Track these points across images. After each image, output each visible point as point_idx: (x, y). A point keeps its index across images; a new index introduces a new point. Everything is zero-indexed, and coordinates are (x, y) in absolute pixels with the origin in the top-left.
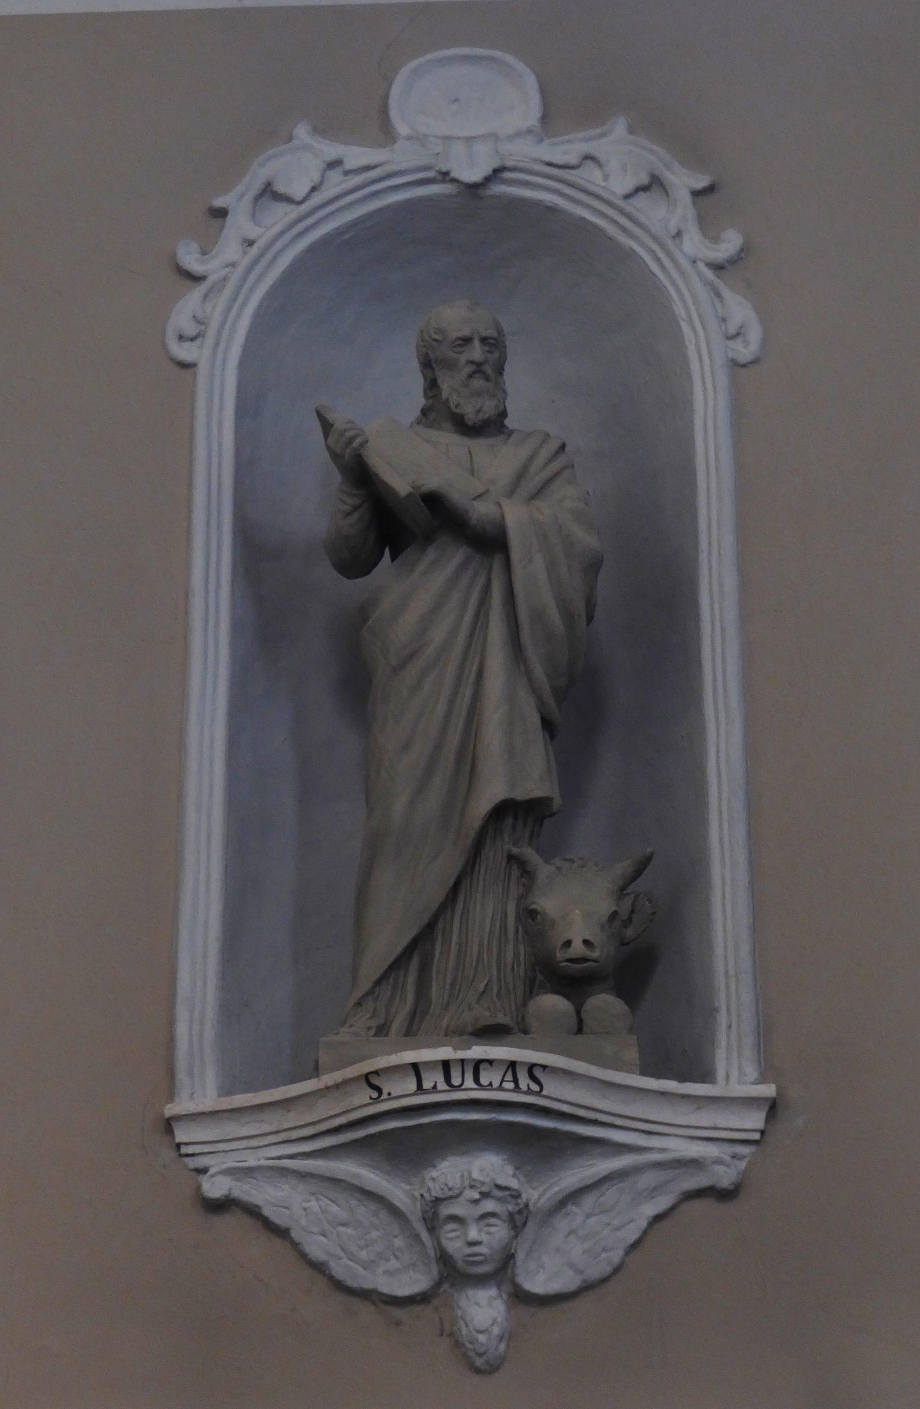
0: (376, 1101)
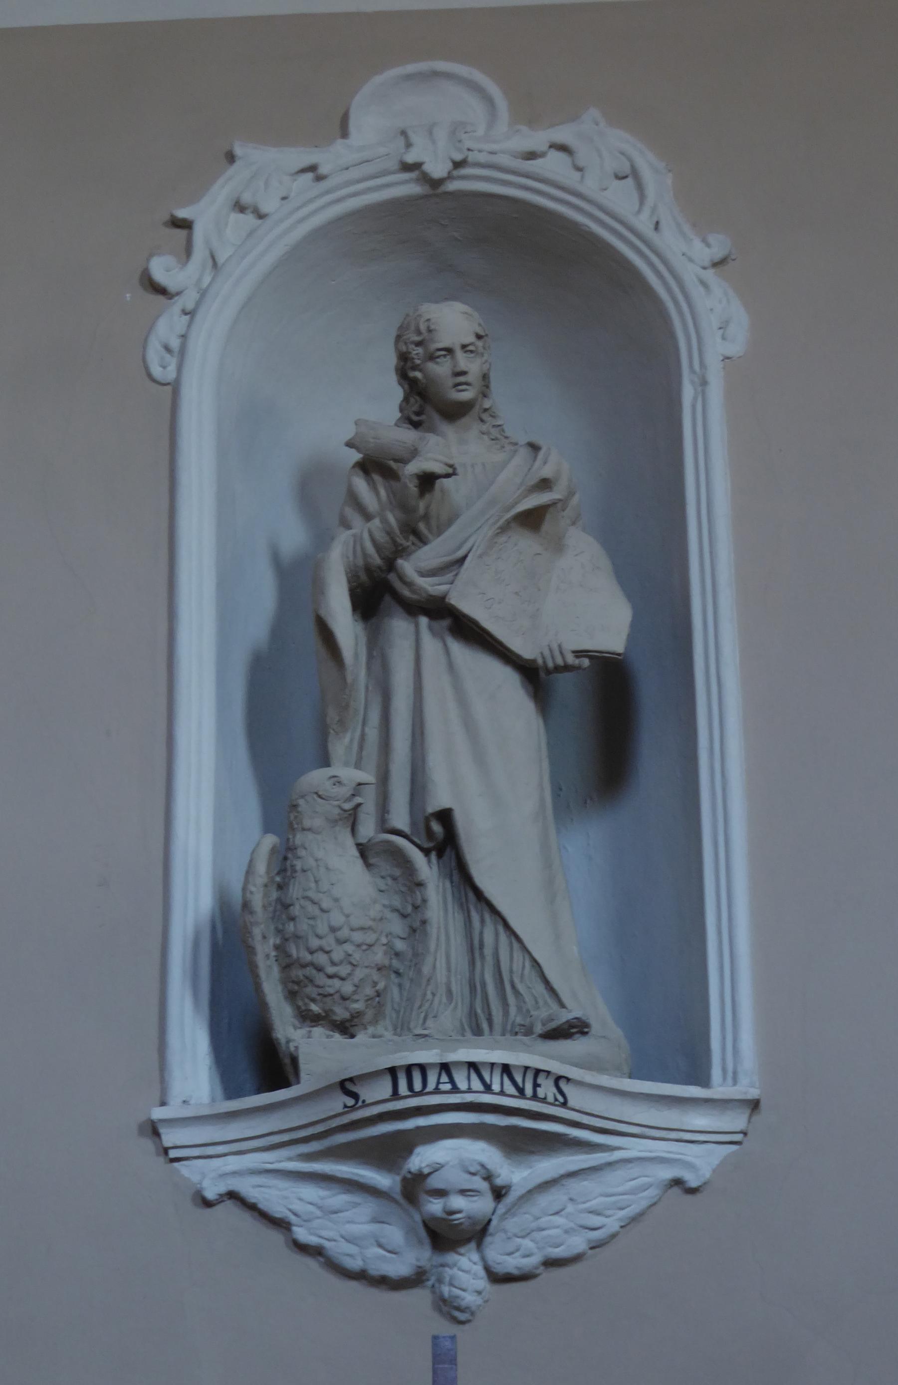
0: (353, 1108)
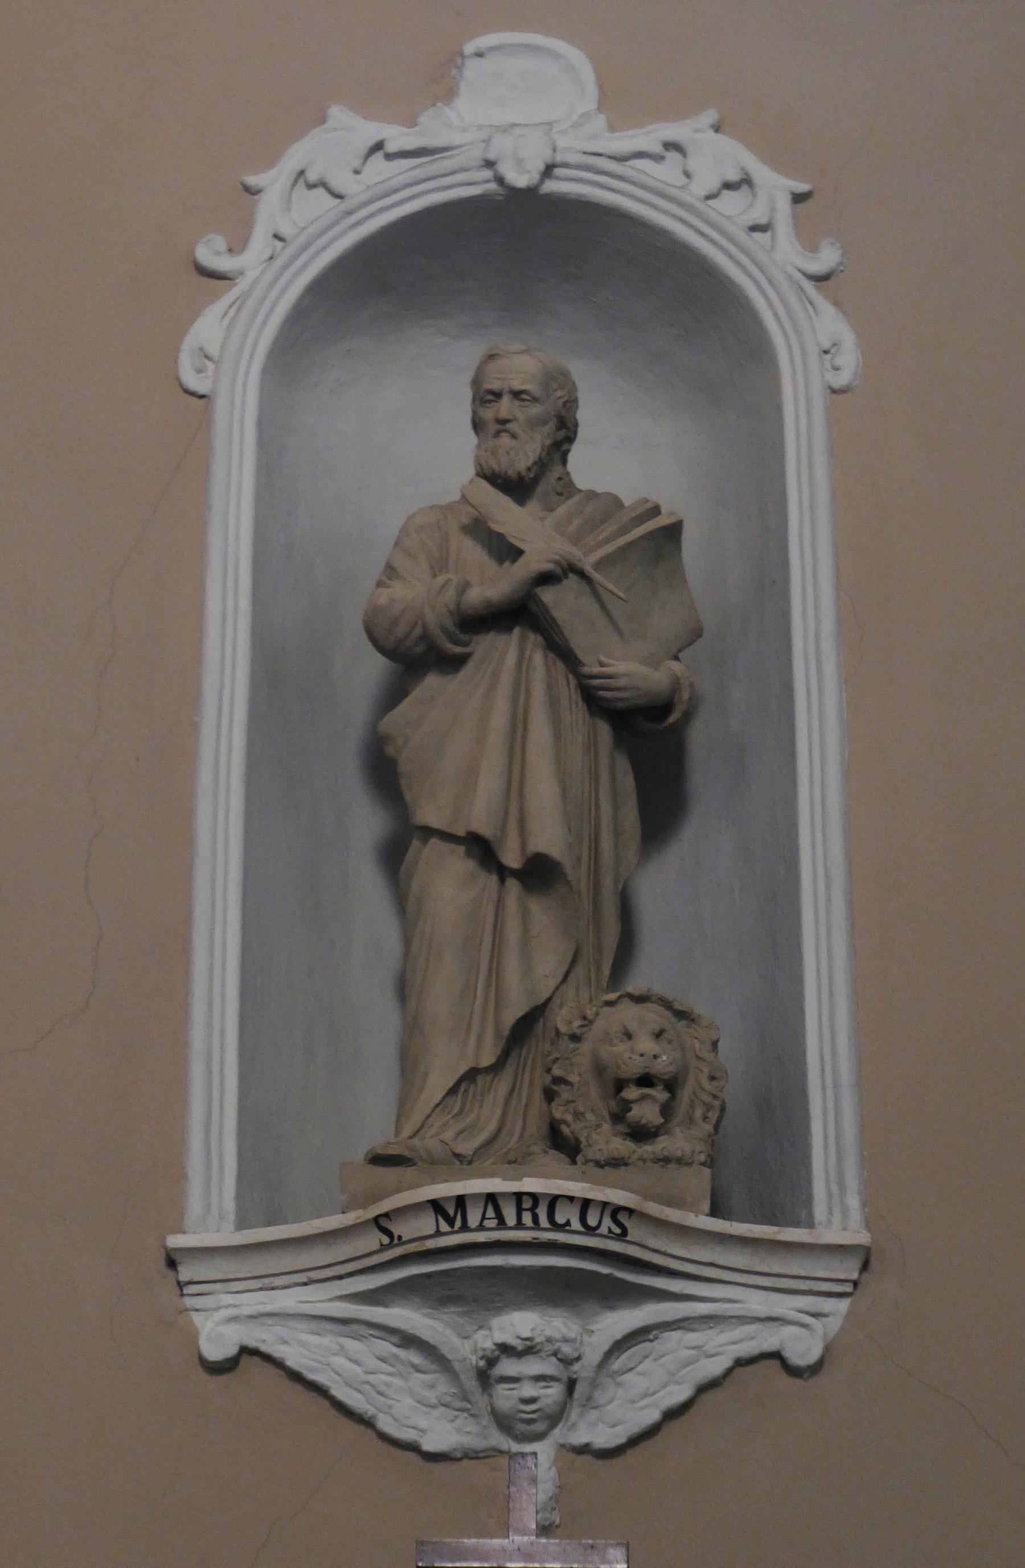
0: (390, 1246)
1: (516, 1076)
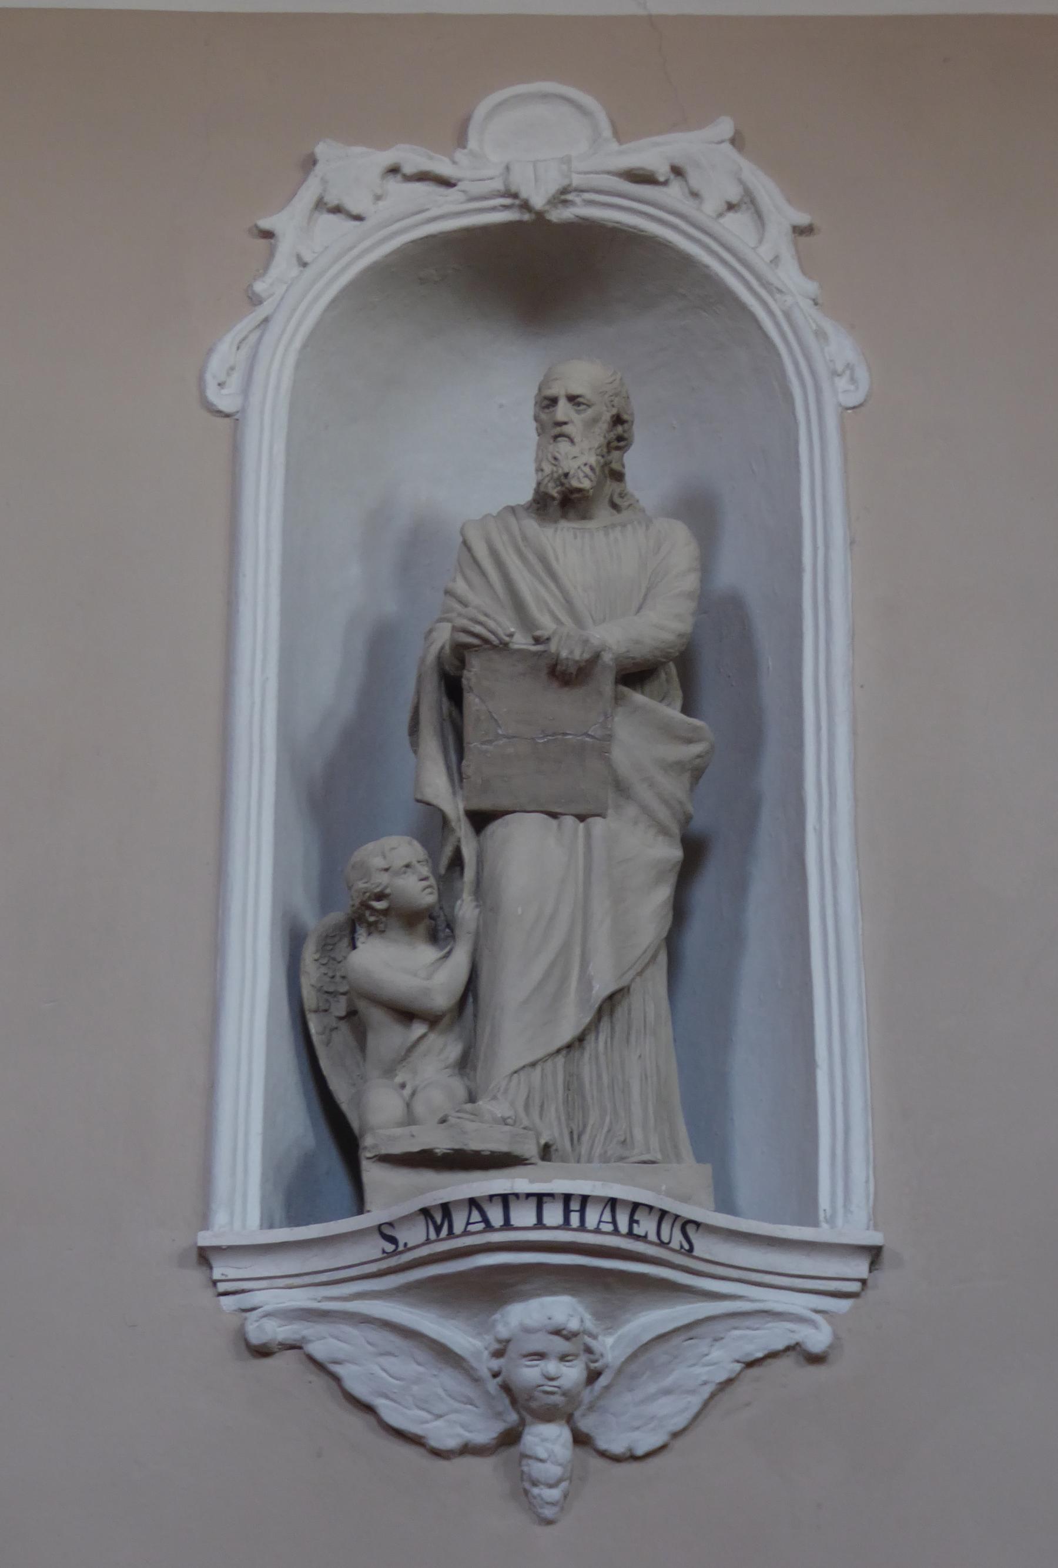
0: (395, 1253)
1: (590, 1153)
